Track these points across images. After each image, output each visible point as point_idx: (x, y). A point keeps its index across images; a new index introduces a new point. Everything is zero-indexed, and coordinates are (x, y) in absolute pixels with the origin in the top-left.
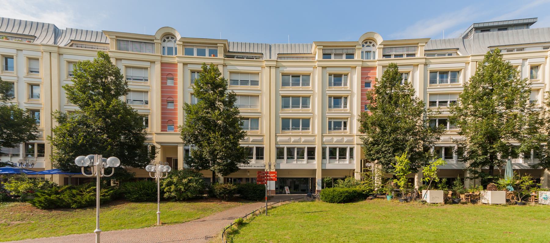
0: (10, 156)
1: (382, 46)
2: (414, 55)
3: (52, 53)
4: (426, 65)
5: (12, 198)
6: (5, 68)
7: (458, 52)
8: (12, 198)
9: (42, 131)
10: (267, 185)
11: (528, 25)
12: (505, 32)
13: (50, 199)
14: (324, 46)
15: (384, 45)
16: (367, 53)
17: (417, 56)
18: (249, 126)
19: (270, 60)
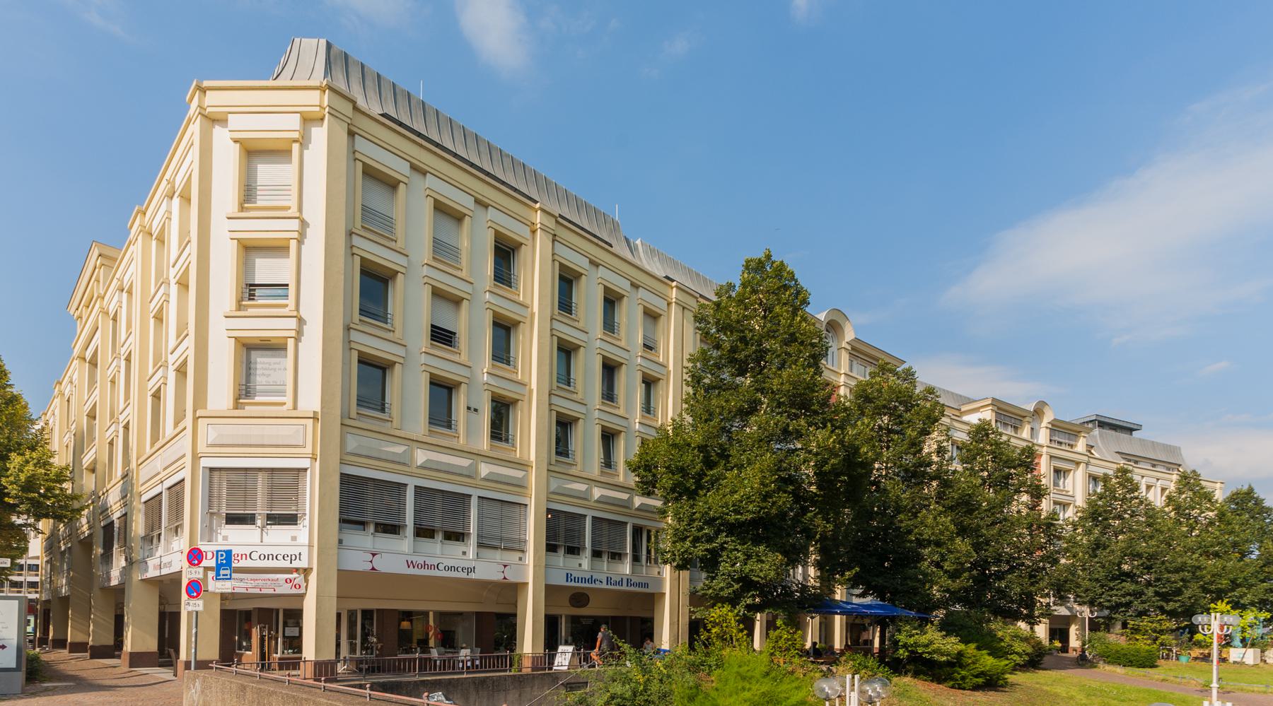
0: (259, 522)
1: (1050, 426)
2: (1072, 446)
3: (685, 310)
4: (1087, 464)
5: (987, 572)
6: (573, 308)
7: (1092, 451)
8: (987, 572)
9: (526, 468)
10: (847, 642)
11: (1130, 430)
12: (1113, 432)
13: (769, 609)
14: (999, 408)
15: (1052, 425)
16: (258, 292)
17: (1075, 450)
18: (473, 529)
19: (292, 289)
